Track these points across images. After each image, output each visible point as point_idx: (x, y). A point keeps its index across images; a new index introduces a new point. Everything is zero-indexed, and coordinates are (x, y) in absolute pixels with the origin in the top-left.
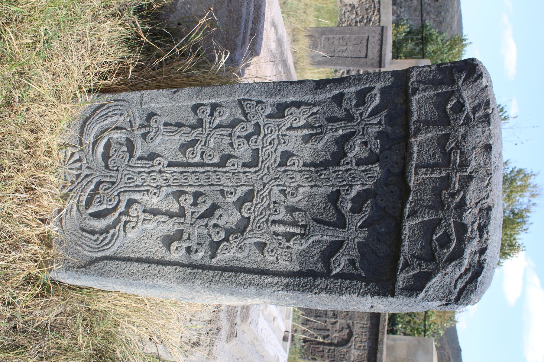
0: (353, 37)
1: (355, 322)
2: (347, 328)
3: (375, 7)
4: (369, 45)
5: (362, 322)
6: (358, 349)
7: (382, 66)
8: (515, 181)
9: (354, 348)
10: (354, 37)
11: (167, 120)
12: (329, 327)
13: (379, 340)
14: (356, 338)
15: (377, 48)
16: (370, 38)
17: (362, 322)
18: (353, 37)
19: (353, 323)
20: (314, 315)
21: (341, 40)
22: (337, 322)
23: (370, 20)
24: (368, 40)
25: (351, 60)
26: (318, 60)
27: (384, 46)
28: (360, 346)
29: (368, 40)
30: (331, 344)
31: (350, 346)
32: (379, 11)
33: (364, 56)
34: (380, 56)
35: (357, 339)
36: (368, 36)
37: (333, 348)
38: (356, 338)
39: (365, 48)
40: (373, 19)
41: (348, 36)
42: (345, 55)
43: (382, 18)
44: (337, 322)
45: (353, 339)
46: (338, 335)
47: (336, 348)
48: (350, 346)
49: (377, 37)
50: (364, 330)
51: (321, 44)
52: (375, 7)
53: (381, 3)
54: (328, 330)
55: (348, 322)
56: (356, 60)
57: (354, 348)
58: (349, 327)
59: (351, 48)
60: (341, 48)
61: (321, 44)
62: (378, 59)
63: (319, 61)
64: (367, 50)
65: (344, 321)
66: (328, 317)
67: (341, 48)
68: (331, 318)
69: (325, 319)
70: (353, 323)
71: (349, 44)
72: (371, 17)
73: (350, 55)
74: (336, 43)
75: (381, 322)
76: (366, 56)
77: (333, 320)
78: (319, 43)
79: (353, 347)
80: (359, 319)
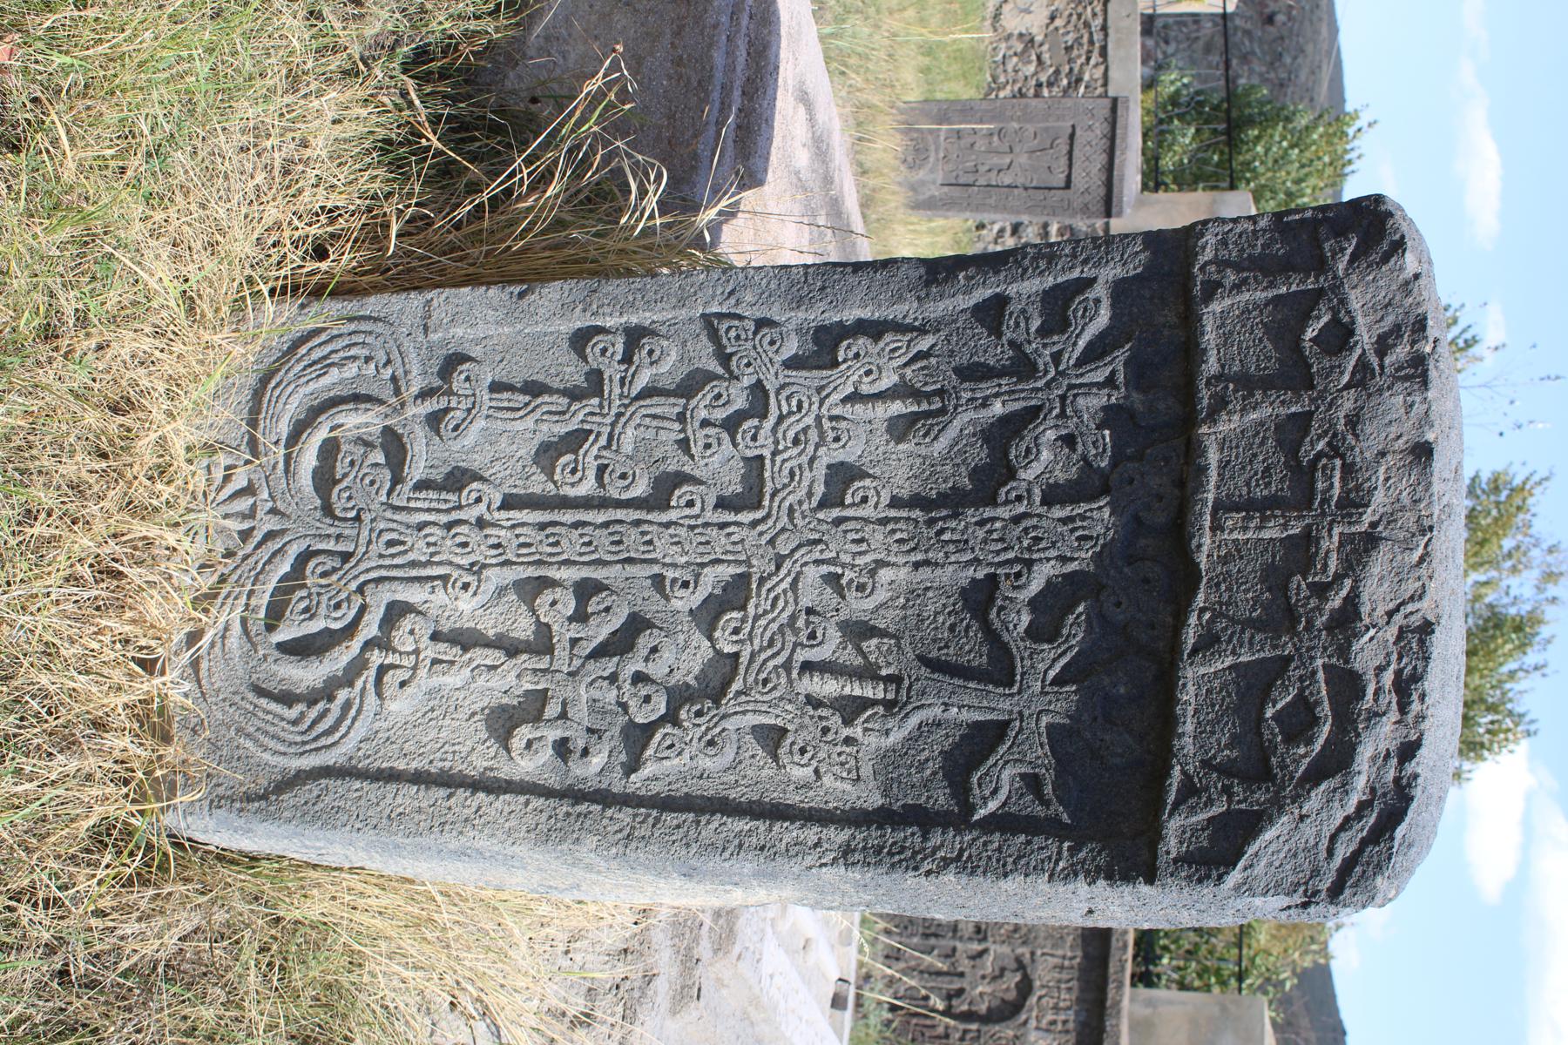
0: (1031, 128)
1: (1039, 952)
2: (1017, 970)
3: (1091, 42)
4: (1076, 153)
5: (1060, 952)
6: (1048, 1031)
7: (1114, 210)
8: (1499, 508)
9: (1037, 1028)
10: (1032, 130)
11: (501, 374)
12: (964, 965)
13: (1109, 1003)
14: (1040, 998)
15: (1100, 160)
16: (1078, 132)
17: (1060, 952)
18: (1031, 128)
19: (1033, 954)
20: (921, 930)
21: (995, 138)
22: (985, 951)
23: (1079, 80)
24: (1072, 136)
25: (1024, 194)
26: (928, 194)
27: (1118, 153)
28: (1053, 1023)
29: (1072, 136)
30: (968, 1016)
31: (1026, 1022)
32: (1104, 52)
33: (1062, 184)
34: (1109, 184)
35: (1044, 1000)
36: (1073, 127)
37: (974, 1027)
38: (1040, 998)
39: (1064, 161)
40: (1086, 77)
41: (1016, 125)
42: (1007, 181)
43: (1111, 74)
44: (985, 951)
45: (1033, 1000)
46: (988, 989)
47: (984, 1028)
48: (1026, 1022)
49: (1100, 128)
50: (1065, 976)
51: (937, 151)
52: (1091, 42)
53: (1110, 31)
54: (962, 975)
55: (1020, 951)
56: (1040, 195)
57: (1037, 1028)
58: (1020, 965)
59: (1023, 159)
60: (996, 160)
61: (937, 151)
62: (1102, 191)
63: (933, 197)
64: (1070, 166)
65: (1006, 949)
66: (961, 939)
67: (996, 160)
68: (970, 939)
69: (952, 943)
70: (1033, 954)
71: (1017, 149)
72: (1081, 72)
73: (1020, 181)
74: (981, 145)
75: (1113, 951)
76: (1068, 185)
77: (976, 947)
78: (932, 148)
79: (1033, 1023)
80: (1049, 943)
